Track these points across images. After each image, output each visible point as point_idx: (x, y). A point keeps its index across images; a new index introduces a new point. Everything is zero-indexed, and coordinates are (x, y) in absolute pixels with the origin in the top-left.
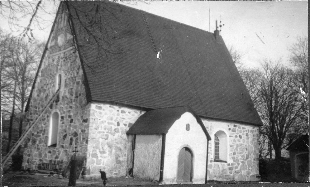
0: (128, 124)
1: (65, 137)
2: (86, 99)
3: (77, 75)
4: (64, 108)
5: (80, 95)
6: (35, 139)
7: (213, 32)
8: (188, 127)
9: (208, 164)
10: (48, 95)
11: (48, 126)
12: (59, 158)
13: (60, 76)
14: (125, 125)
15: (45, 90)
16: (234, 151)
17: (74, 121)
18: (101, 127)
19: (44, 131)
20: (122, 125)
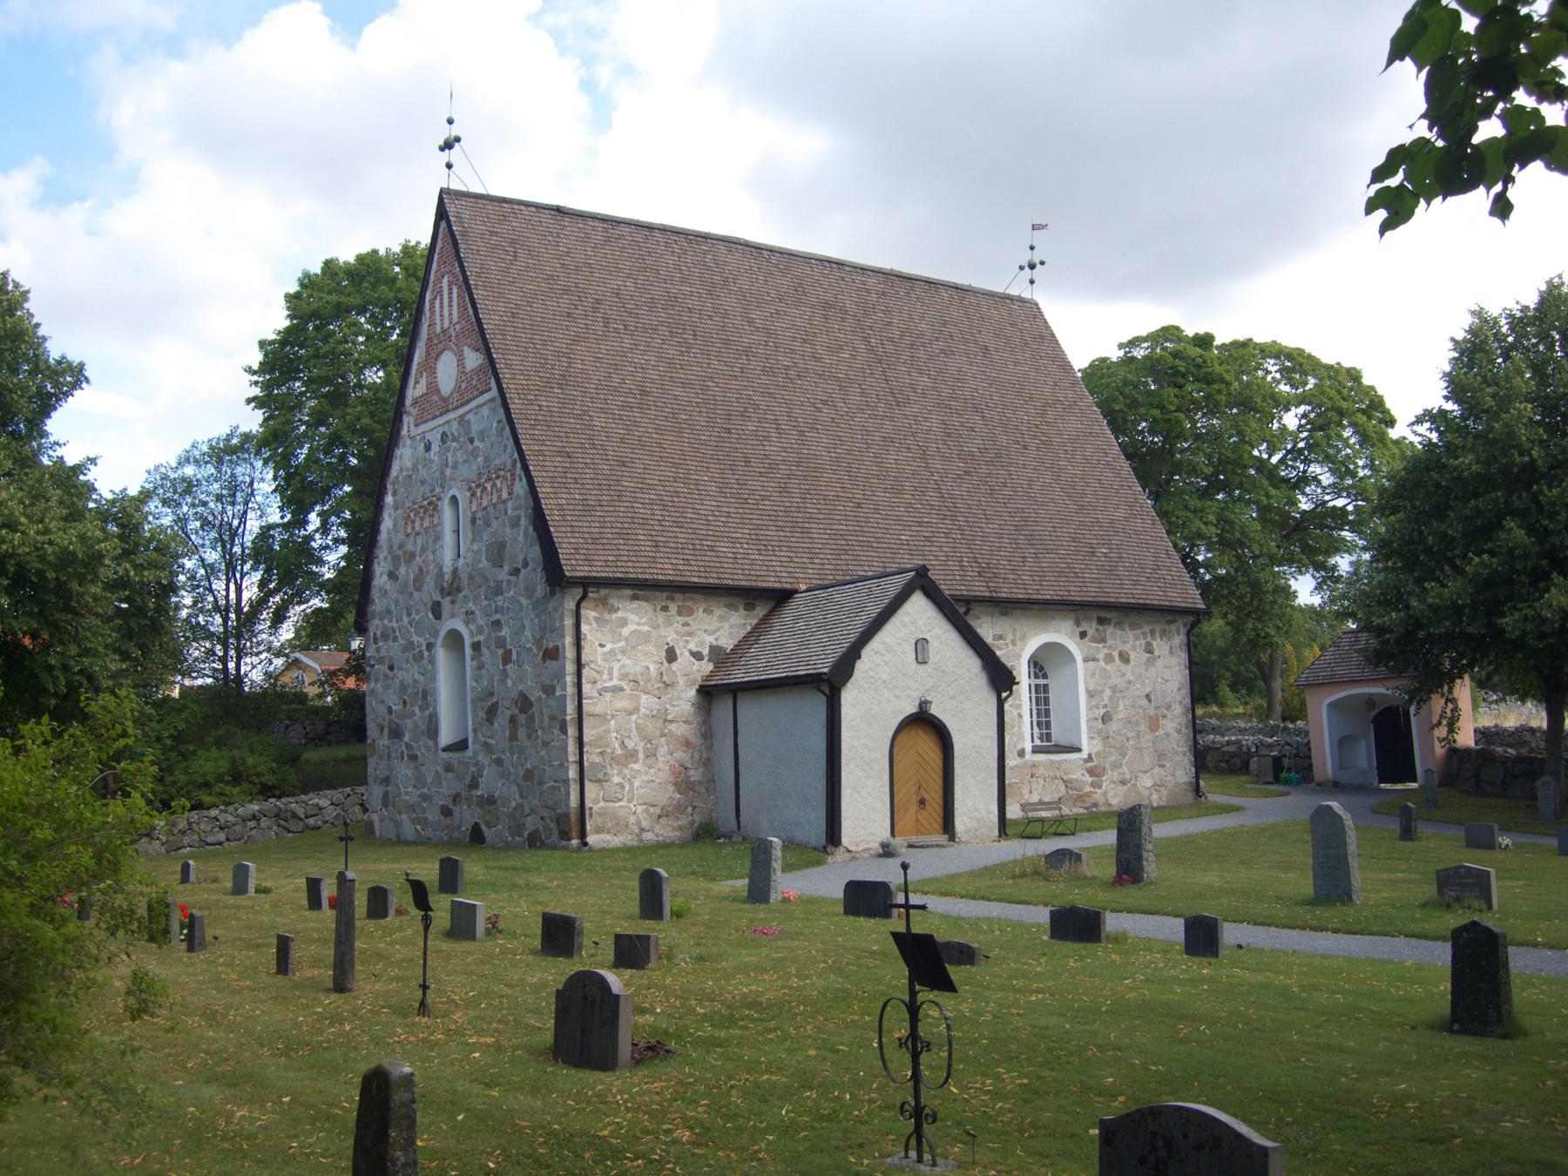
0: (706, 652)
1: (492, 712)
4: (477, 612)
6: (398, 725)
7: (1407, 59)
8: (921, 646)
10: (421, 569)
11: (433, 677)
13: (454, 500)
14: (697, 656)
15: (412, 555)
17: (514, 657)
18: (611, 674)
19: (425, 693)
20: (684, 658)
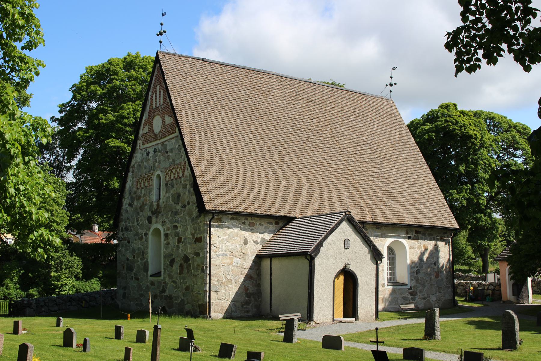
0: (259, 241)
2: (197, 210)
3: (183, 175)
5: (189, 204)
8: (346, 243)
9: (379, 289)
12: (167, 292)
13: (159, 176)
16: (417, 269)
